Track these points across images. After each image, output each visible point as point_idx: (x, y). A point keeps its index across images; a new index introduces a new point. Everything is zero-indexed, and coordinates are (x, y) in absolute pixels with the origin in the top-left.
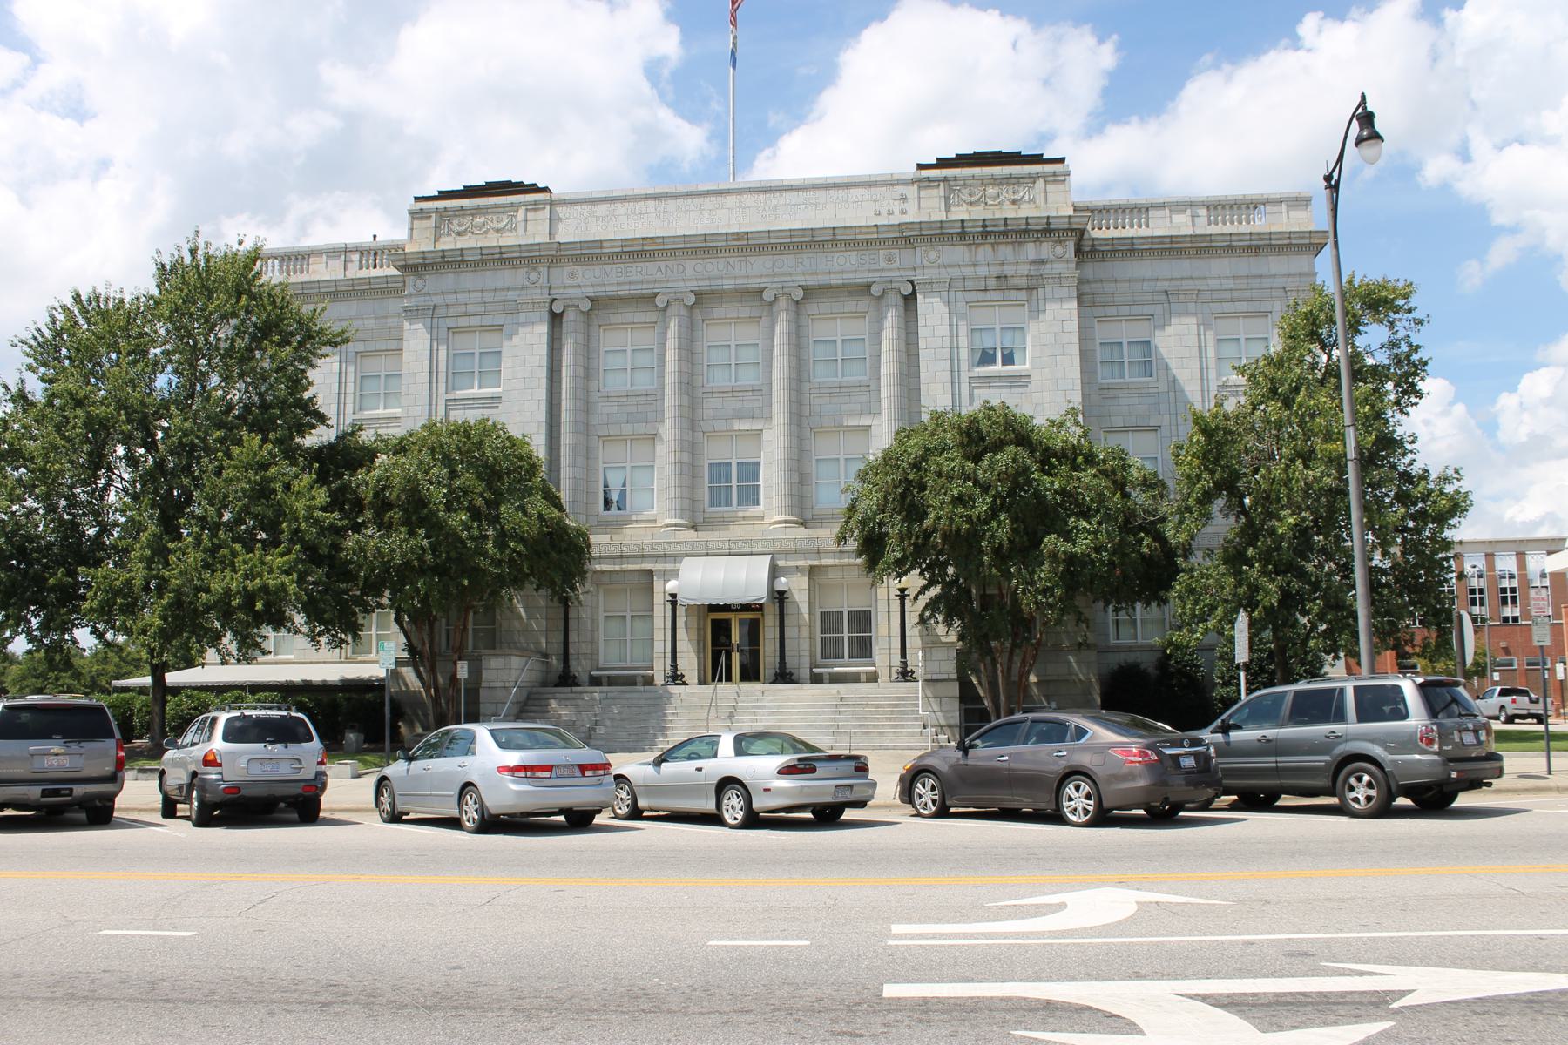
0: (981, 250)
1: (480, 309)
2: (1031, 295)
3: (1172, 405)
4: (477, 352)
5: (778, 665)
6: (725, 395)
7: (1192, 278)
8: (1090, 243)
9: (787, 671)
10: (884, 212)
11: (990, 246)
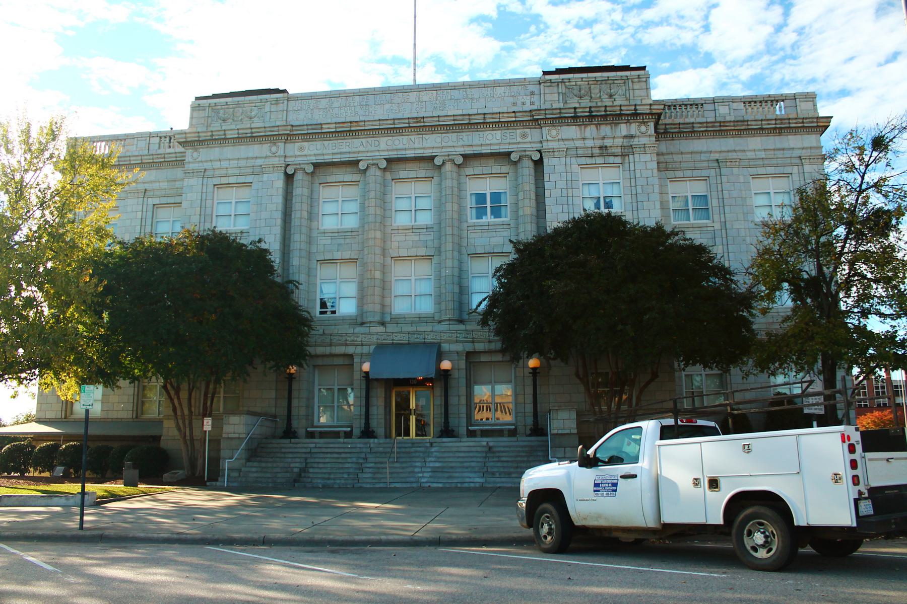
0: (588, 129)
1: (237, 171)
2: (624, 160)
3: (724, 239)
4: (234, 201)
5: (443, 425)
6: (407, 231)
7: (735, 151)
8: (664, 127)
9: (370, 430)
10: (519, 103)
11: (594, 126)
